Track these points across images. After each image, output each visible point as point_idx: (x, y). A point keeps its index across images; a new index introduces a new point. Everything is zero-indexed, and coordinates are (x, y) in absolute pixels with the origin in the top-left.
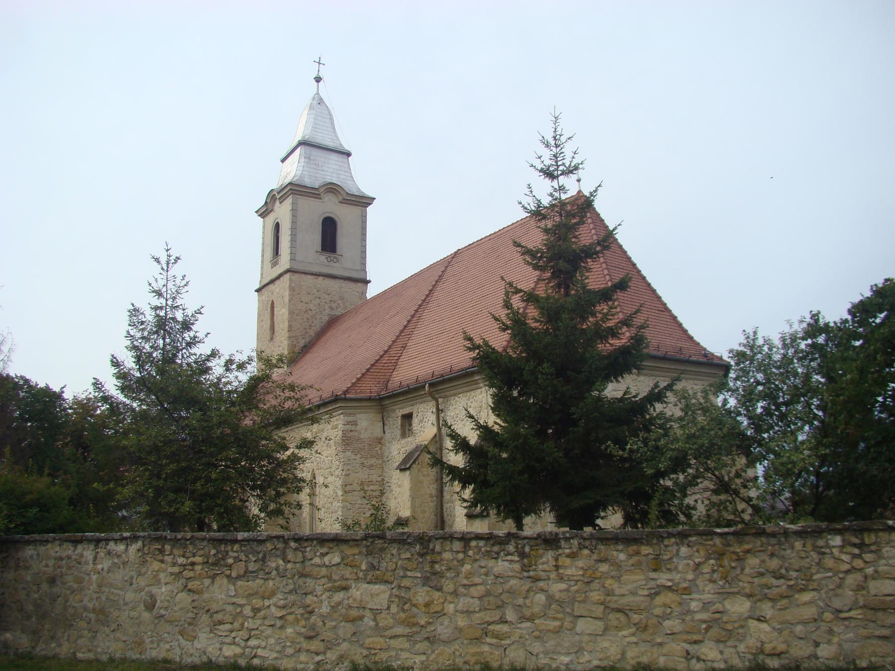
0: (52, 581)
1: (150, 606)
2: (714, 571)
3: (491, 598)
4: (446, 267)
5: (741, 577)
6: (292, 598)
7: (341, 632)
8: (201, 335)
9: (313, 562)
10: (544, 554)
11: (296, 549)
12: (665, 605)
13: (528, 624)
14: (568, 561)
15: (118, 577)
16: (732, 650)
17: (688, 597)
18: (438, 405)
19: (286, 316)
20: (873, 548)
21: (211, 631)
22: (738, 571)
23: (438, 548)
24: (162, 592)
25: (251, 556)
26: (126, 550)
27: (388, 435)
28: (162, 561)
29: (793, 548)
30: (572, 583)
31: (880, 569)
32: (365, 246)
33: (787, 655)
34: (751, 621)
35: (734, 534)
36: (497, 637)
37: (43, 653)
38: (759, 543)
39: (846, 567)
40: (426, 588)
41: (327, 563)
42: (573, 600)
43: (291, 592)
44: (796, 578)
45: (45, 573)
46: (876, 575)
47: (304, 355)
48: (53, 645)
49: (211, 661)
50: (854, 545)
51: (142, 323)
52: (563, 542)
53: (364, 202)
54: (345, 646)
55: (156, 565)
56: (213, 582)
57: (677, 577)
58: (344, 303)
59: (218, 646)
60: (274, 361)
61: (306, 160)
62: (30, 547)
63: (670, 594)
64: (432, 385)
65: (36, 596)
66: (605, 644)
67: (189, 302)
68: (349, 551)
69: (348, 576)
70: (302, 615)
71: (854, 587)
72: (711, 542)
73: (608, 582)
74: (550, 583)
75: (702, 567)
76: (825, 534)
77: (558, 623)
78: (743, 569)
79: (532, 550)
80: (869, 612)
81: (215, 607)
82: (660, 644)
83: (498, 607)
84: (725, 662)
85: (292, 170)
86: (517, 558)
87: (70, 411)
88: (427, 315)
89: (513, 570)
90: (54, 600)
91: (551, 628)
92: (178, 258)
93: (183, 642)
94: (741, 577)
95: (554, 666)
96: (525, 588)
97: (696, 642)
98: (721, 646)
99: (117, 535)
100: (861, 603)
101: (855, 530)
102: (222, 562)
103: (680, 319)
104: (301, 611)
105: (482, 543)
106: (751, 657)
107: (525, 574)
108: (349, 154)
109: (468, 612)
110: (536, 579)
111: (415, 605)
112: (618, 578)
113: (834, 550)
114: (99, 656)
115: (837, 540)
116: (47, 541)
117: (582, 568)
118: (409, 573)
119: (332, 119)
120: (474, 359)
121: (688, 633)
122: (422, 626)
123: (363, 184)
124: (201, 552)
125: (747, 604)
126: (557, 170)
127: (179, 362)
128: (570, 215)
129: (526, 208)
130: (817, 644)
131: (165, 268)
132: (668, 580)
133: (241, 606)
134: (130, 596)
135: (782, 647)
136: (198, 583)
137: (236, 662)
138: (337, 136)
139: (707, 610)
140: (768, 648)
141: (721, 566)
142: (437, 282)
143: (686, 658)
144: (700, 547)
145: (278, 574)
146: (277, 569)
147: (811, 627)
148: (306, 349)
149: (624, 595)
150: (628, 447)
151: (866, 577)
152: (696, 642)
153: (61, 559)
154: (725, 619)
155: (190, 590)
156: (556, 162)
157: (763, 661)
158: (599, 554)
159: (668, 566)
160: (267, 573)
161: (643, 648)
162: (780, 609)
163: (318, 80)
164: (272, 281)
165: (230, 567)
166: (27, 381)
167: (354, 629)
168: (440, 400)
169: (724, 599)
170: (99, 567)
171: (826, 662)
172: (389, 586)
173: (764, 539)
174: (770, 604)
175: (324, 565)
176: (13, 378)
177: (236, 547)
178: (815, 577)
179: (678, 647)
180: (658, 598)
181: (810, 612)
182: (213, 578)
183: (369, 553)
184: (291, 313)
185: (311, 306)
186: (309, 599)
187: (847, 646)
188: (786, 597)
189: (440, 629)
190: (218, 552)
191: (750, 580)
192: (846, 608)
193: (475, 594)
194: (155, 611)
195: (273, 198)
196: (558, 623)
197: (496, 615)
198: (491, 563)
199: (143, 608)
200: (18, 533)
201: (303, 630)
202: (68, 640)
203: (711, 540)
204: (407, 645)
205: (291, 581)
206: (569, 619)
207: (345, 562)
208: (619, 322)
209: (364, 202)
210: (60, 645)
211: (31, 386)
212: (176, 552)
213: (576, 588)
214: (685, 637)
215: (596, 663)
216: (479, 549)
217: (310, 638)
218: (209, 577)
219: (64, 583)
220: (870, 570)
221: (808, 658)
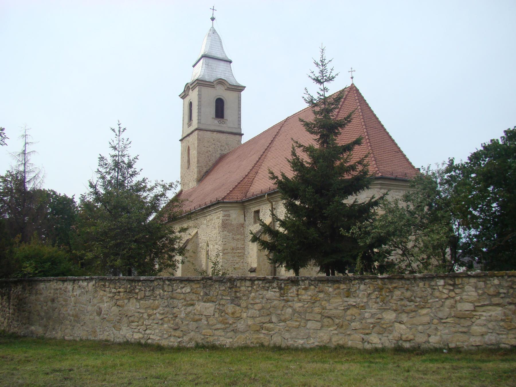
0: (53, 300)
1: (99, 313)
2: (377, 298)
3: (264, 310)
4: (281, 127)
5: (392, 301)
6: (167, 309)
7: (190, 327)
8: (138, 170)
9: (177, 291)
10: (291, 288)
11: (169, 285)
12: (352, 315)
13: (283, 324)
14: (303, 292)
15: (84, 298)
16: (386, 338)
17: (364, 311)
18: (272, 206)
19: (196, 155)
20: (460, 286)
21: (128, 326)
22: (390, 297)
23: (238, 285)
24: (105, 306)
25: (147, 288)
26: (88, 285)
27: (247, 222)
28: (105, 291)
29: (418, 286)
30: (306, 303)
31: (464, 297)
32: (240, 114)
33: (414, 341)
34: (396, 323)
35: (388, 278)
36: (267, 330)
37: (49, 336)
38: (401, 283)
39: (445, 296)
40: (232, 305)
41: (184, 292)
42: (306, 312)
43: (166, 306)
44: (420, 302)
45: (49, 297)
46: (461, 300)
47: (206, 177)
48: (54, 332)
49: (128, 341)
50: (450, 285)
51: (106, 164)
52: (301, 282)
53: (239, 89)
54: (192, 333)
55: (102, 293)
56: (129, 301)
57: (358, 300)
58: (228, 147)
59: (131, 333)
60: (168, 186)
61: (207, 66)
62: (42, 283)
63: (355, 309)
64: (269, 195)
65: (46, 308)
66: (322, 334)
67: (131, 153)
68: (195, 286)
69: (194, 298)
70: (172, 318)
71: (449, 307)
72: (376, 283)
73: (323, 303)
74: (294, 303)
75: (371, 295)
76: (435, 279)
77: (298, 323)
78: (392, 297)
79: (285, 286)
80: (457, 319)
81: (130, 314)
82: (349, 335)
83: (268, 315)
84: (382, 344)
85: (199, 72)
86: (277, 290)
87: (79, 209)
88: (269, 155)
89: (275, 296)
90: (54, 310)
91: (294, 326)
92: (125, 129)
93: (114, 331)
94: (392, 301)
95: (296, 345)
96: (282, 305)
97: (367, 334)
98: (380, 336)
99: (83, 278)
100: (453, 315)
101: (450, 277)
102: (133, 291)
103: (408, 156)
104: (171, 316)
105: (260, 282)
106: (395, 342)
107: (282, 298)
109: (253, 317)
110: (288, 301)
111: (227, 314)
112: (328, 301)
113: (440, 287)
114: (75, 338)
115: (441, 282)
116: (50, 281)
117: (310, 295)
118: (224, 297)
119: (221, 42)
120: (275, 184)
121: (363, 329)
124: (123, 286)
125: (394, 315)
126: (323, 79)
127: (126, 185)
128: (330, 104)
129: (306, 100)
130: (429, 336)
131: (118, 134)
133: (143, 313)
134: (90, 308)
135: (411, 337)
136: (122, 302)
137: (140, 341)
138: (224, 52)
139: (373, 318)
140: (404, 337)
141: (381, 295)
142: (276, 136)
143: (362, 342)
144: (371, 285)
145: (160, 297)
146: (160, 295)
147: (427, 327)
148: (207, 173)
149: (331, 310)
150: (351, 231)
151: (456, 301)
152: (367, 334)
153: (57, 289)
154: (382, 322)
155: (118, 305)
156: (323, 74)
157: (402, 344)
158: (319, 288)
159: (354, 295)
160: (155, 297)
161: (341, 336)
162: (411, 318)
163: (213, 19)
164: (188, 135)
165: (137, 293)
166: (55, 193)
167: (197, 325)
168: (273, 203)
169: (382, 312)
170: (75, 293)
171: (434, 345)
172: (214, 303)
173: (403, 281)
174: (406, 315)
175: (182, 293)
176: (47, 191)
177: (140, 284)
178: (429, 301)
179: (358, 336)
180: (348, 311)
181: (426, 319)
182: (129, 299)
183: (205, 287)
184: (199, 153)
185: (210, 149)
186: (175, 310)
187: (444, 337)
188: (414, 311)
189: (239, 326)
190: (131, 286)
191: (395, 302)
192: (445, 317)
193: (257, 308)
194: (102, 315)
195: (188, 88)
196: (298, 323)
197: (267, 319)
198: (265, 292)
199: (96, 314)
200: (41, 276)
201: (172, 325)
202: (61, 330)
204: (223, 334)
205: (166, 301)
206: (303, 321)
207: (192, 292)
208: (356, 162)
209: (239, 89)
210: (57, 333)
211: (57, 195)
212: (111, 286)
213: (307, 305)
214: (362, 331)
215: (316, 344)
216: (259, 285)
217: (176, 329)
218: (127, 299)
219: (58, 302)
220: (458, 298)
221: (424, 343)
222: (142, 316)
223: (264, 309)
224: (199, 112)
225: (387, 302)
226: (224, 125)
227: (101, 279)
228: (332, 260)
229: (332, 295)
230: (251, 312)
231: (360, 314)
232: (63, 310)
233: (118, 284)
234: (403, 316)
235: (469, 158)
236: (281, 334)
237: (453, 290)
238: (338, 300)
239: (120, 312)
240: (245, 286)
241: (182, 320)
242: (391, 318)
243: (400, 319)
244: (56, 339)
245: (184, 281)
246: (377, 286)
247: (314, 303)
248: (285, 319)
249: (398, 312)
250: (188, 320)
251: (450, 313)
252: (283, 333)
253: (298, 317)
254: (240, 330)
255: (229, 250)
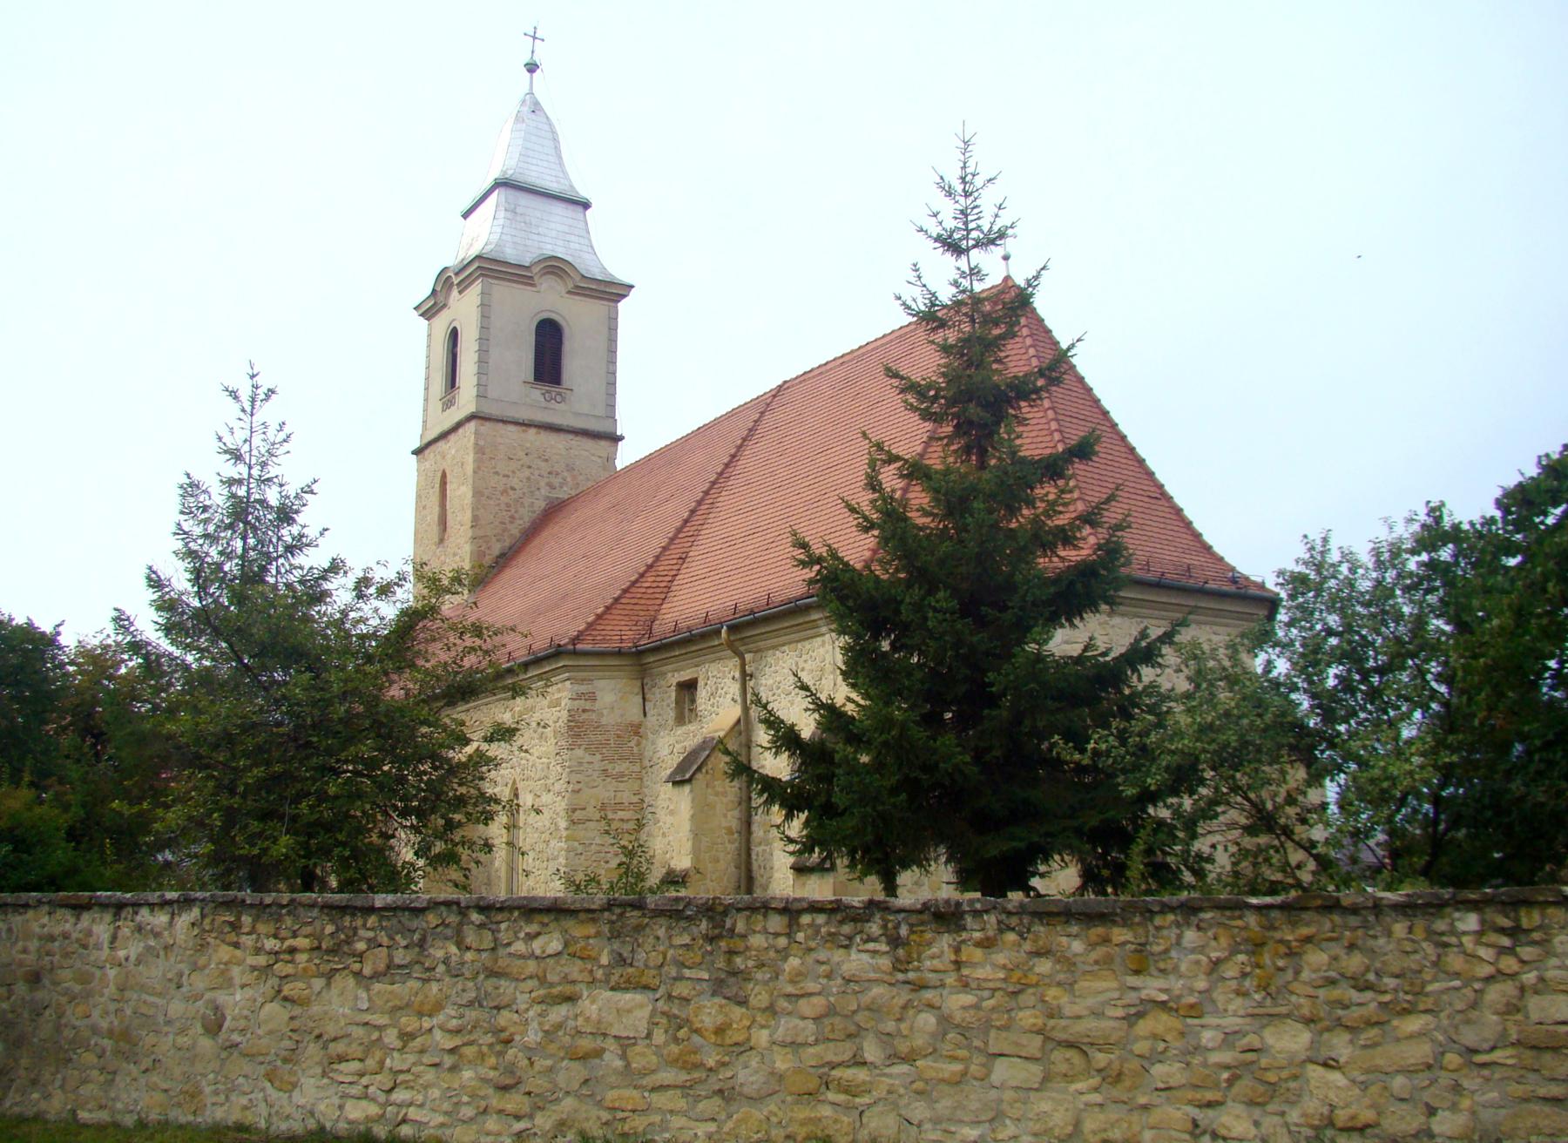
0: (35, 978)
1: (214, 1027)
2: (1244, 975)
3: (837, 1020)
4: (762, 413)
5: (1295, 986)
6: (472, 1014)
9: (512, 949)
11: (482, 926)
12: (1155, 1037)
13: (904, 1068)
14: (978, 954)
15: (155, 972)
16: (1276, 1119)
17: (1196, 1021)
18: (743, 665)
20: (1536, 936)
21: (324, 1074)
22: (1289, 975)
23: (740, 927)
24: (235, 1001)
25: (398, 938)
26: (171, 923)
27: (652, 719)
28: (236, 945)
29: (1389, 934)
30: (986, 994)
31: (1550, 974)
34: (1310, 1067)
35: (1282, 907)
36: (846, 1092)
37: (17, 1109)
38: (1328, 925)
39: (1487, 970)
40: (718, 1000)
41: (538, 952)
42: (987, 1026)
43: (470, 1004)
44: (1395, 990)
45: (21, 964)
46: (1540, 986)
47: (500, 572)
48: (35, 1096)
49: (323, 1128)
50: (1502, 931)
51: (205, 509)
52: (969, 919)
53: (612, 292)
54: (568, 1103)
55: (225, 952)
56: (328, 985)
57: (1177, 985)
58: (574, 478)
59: (336, 1101)
60: (446, 582)
61: (509, 215)
63: (1164, 1017)
64: (733, 629)
66: (1045, 1106)
67: (291, 472)
68: (578, 930)
69: (575, 975)
70: (491, 1045)
71: (1500, 1007)
72: (1239, 923)
73: (1052, 992)
74: (945, 992)
75: (1222, 967)
76: (1448, 910)
77: (958, 1067)
78: (1297, 973)
80: (1529, 1053)
81: (331, 1030)
83: (850, 1036)
86: (884, 947)
87: (71, 669)
89: (876, 969)
90: (38, 1013)
91: (946, 1075)
97: (1210, 1105)
98: (1257, 1112)
99: (154, 897)
101: (1503, 903)
102: (346, 948)
104: (489, 1039)
105: (821, 919)
107: (900, 976)
108: (586, 205)
109: (794, 1045)
110: (920, 986)
111: (697, 1031)
112: (1069, 986)
113: (1465, 939)
115: (1470, 922)
116: (26, 906)
117: (1004, 967)
118: (687, 973)
119: (555, 140)
120: (811, 582)
122: (711, 1070)
123: (613, 262)
124: (309, 929)
125: (1305, 1037)
127: (272, 580)
129: (909, 308)
130: (1432, 1111)
131: (248, 409)
132: (1161, 990)
133: (379, 1028)
134: (176, 1008)
135: (1367, 1115)
136: (301, 985)
137: (369, 1130)
138: (564, 172)
139: (1232, 1047)
140: (1342, 1116)
141: (1258, 966)
142: (744, 440)
143: (1192, 1134)
144: (1221, 931)
145: (448, 971)
146: (446, 961)
147: (1422, 1079)
148: (505, 559)
149: (1079, 1017)
150: (1091, 745)
151: (1522, 989)
152: (1210, 1105)
153: (52, 938)
154: (1264, 1062)
155: (286, 999)
156: (966, 223)
159: (1162, 965)
161: (1114, 1113)
162: (1365, 1047)
163: (532, 68)
164: (444, 436)
167: (584, 1074)
168: (748, 657)
169: (1263, 1027)
170: (122, 954)
172: (651, 995)
173: (1337, 918)
174: (1346, 1036)
175: (533, 956)
177: (372, 920)
178: (1429, 988)
181: (1420, 1052)
182: (329, 976)
183: (615, 935)
184: (477, 493)
185: (515, 482)
186: (505, 1018)
187: (1486, 1115)
188: (1377, 1023)
189: (742, 1075)
190: (338, 930)
191: (1311, 991)
192: (1486, 1046)
194: (223, 1035)
195: (446, 284)
196: (958, 1067)
197: (845, 1051)
198: (838, 955)
199: (200, 1030)
201: (492, 1074)
202: (62, 1087)
203: (1240, 917)
204: (682, 1104)
205: (471, 984)
206: (979, 1059)
207: (570, 950)
208: (1077, 518)
209: (612, 292)
210: (47, 1096)
212: (262, 928)
213: (992, 1002)
214: (1190, 1095)
217: (505, 1088)
218: (322, 975)
219: (56, 983)
220: (1530, 977)
221: (1415, 1136)
222: (380, 1039)
223: (836, 1014)
224: (483, 361)
225: (1278, 992)
226: (562, 406)
227: (223, 903)
228: (1015, 844)
229: (1080, 966)
230: (785, 1027)
231: (1182, 1034)
232: (73, 1015)
233: (288, 921)
234: (1335, 1041)
235: (1499, 504)
236: (896, 1105)
237: (1510, 951)
238: (1104, 985)
239: (296, 1024)
240: (765, 931)
241: (530, 1052)
242: (1294, 1047)
243: (1324, 1053)
244: (46, 1122)
245: (540, 911)
246: (1244, 934)
247: (1015, 994)
248: (913, 1050)
249: (1320, 1026)
250: (552, 1056)
251: (1504, 1033)
252: (905, 1100)
253: (958, 1046)
254: (746, 1090)
255: (592, 812)
